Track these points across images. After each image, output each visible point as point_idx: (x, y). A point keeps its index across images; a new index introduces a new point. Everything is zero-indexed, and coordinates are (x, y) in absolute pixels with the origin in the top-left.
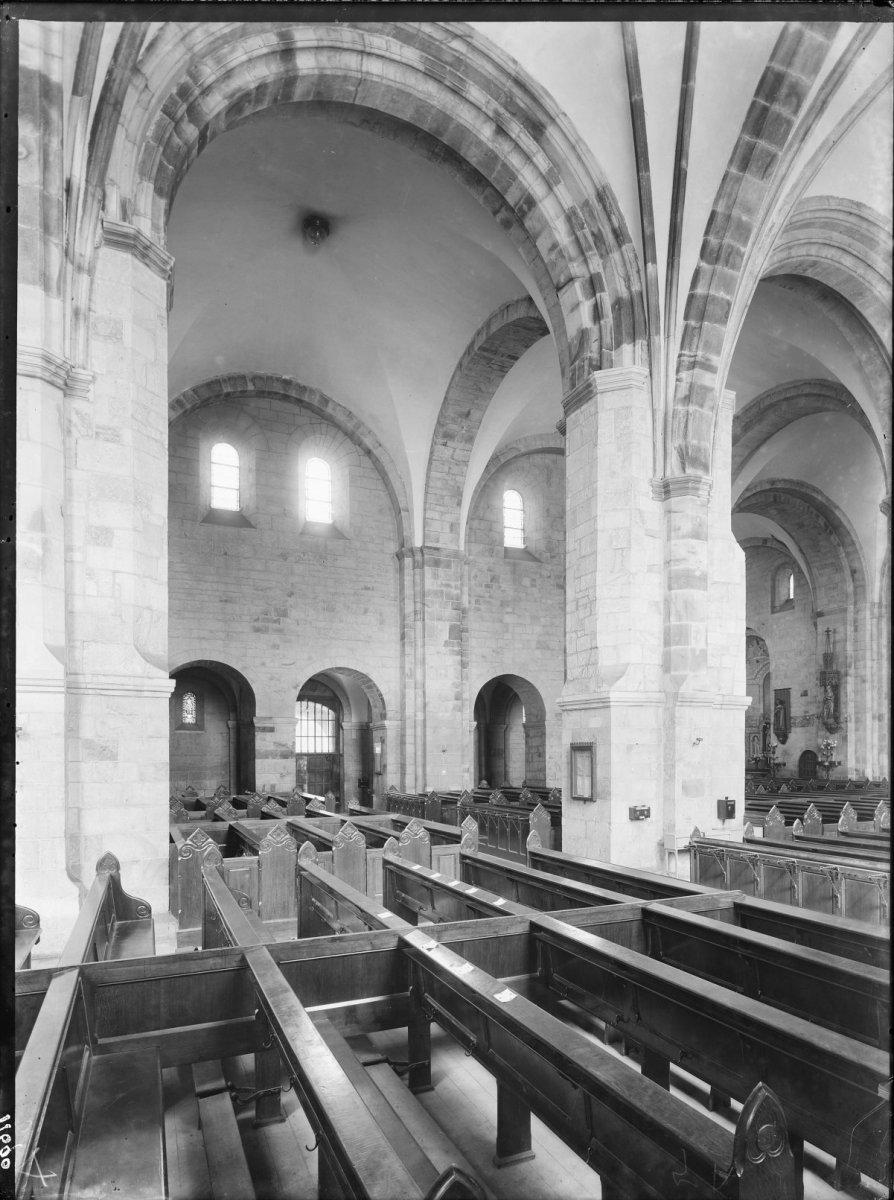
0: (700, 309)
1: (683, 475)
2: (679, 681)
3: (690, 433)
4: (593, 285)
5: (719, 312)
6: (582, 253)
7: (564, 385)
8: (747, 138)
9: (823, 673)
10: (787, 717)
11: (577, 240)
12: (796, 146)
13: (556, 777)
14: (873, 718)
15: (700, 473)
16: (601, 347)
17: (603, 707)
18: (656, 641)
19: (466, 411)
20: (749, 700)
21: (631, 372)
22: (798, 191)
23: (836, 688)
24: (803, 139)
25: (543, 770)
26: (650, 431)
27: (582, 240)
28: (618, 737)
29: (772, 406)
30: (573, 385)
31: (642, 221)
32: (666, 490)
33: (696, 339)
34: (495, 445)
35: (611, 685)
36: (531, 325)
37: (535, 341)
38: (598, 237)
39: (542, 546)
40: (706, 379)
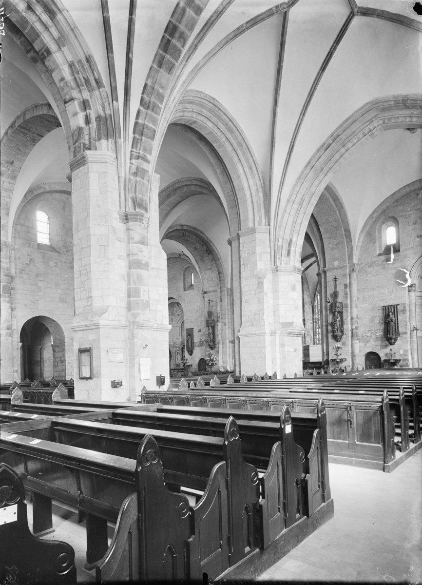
0: (140, 130)
1: (134, 212)
2: (135, 316)
3: (138, 192)
4: (85, 105)
5: (150, 134)
6: (78, 86)
7: (70, 155)
8: (161, 52)
9: (207, 321)
10: (192, 342)
11: (75, 79)
12: (184, 63)
13: (71, 374)
14: (230, 342)
15: (143, 212)
16: (90, 139)
17: (96, 328)
18: (124, 295)
19: (11, 160)
20: (170, 326)
21: (107, 155)
22: (185, 85)
23: (213, 328)
24: (187, 60)
25: (64, 370)
26: (118, 186)
27: (78, 80)
28: (104, 344)
29: (179, 187)
30: (75, 156)
31: (110, 80)
32: (126, 218)
33: (139, 145)
34: (31, 182)
35: (100, 316)
36: (50, 119)
37: (54, 129)
38: (87, 81)
39: (61, 244)
40: (145, 166)
